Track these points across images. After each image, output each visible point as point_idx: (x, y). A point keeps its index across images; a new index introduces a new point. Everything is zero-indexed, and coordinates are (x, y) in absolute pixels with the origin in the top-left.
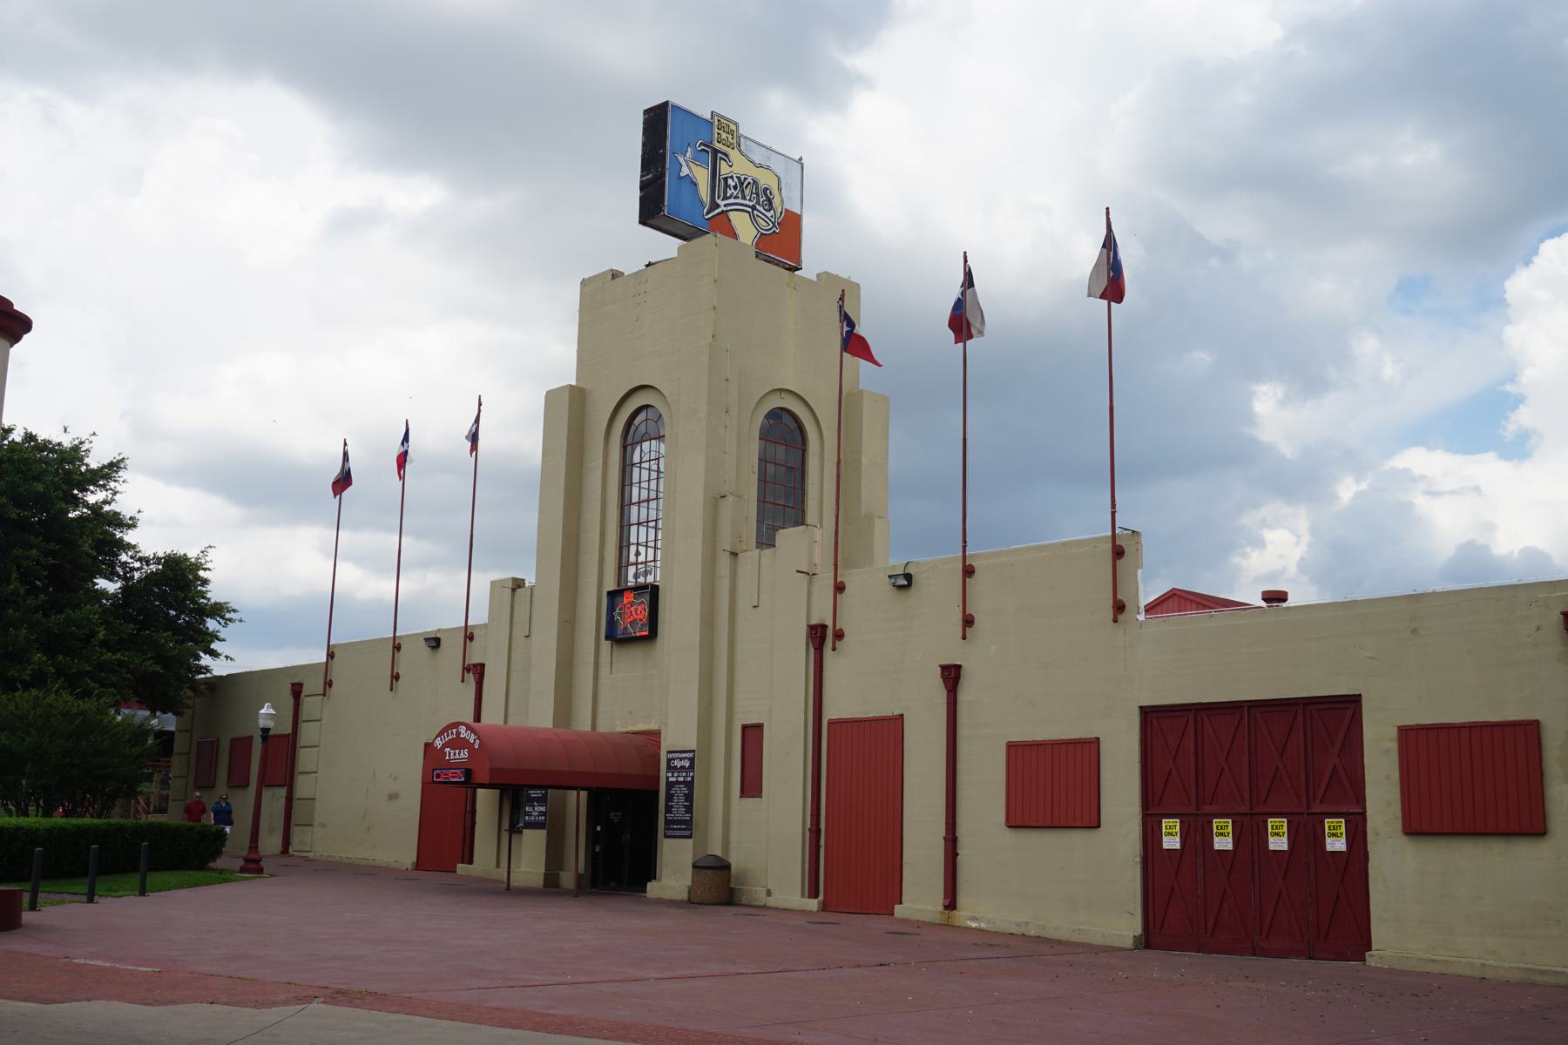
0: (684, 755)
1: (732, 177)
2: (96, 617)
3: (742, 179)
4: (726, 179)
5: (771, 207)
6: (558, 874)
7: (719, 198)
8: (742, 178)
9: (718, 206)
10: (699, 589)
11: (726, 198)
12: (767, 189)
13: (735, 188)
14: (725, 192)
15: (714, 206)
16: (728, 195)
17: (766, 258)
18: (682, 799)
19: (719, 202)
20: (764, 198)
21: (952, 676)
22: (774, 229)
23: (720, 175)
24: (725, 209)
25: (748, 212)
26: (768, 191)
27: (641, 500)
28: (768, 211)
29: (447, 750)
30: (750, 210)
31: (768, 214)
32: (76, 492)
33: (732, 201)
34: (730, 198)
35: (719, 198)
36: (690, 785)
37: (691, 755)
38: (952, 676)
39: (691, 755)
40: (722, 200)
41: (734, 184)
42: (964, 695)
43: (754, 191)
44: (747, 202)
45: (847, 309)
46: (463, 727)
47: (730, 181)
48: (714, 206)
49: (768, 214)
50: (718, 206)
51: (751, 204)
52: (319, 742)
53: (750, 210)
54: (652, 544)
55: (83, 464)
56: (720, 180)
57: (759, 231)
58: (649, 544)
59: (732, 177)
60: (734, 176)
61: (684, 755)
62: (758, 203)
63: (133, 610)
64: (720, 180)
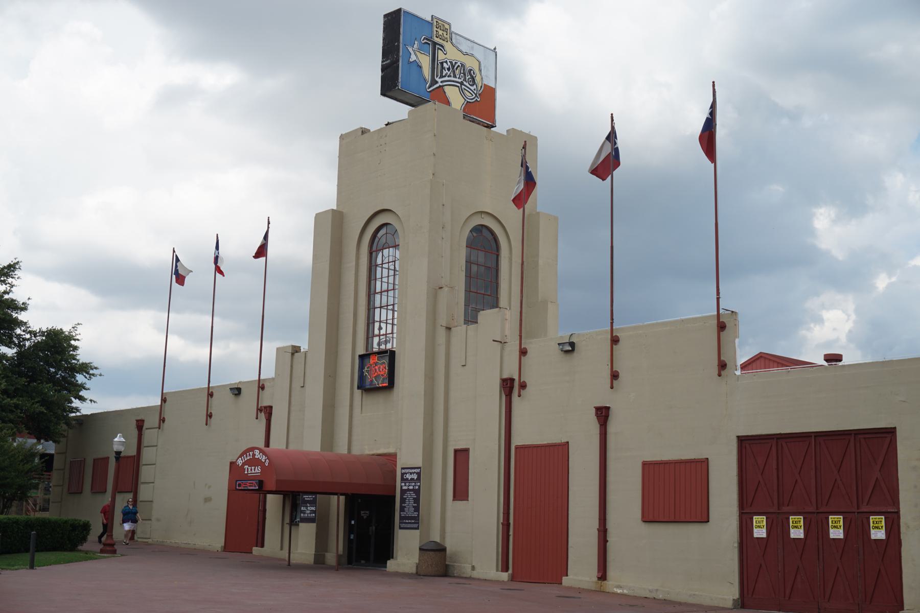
0: (413, 471)
4: (442, 63)
9: (437, 82)
14: (442, 72)
18: (412, 502)
19: (437, 79)
20: (469, 77)
21: (603, 414)
26: (472, 72)
29: (246, 467)
34: (445, 76)
36: (417, 492)
37: (418, 470)
38: (603, 414)
39: (418, 470)
42: (612, 428)
43: (462, 72)
46: (257, 451)
47: (445, 65)
61: (413, 471)
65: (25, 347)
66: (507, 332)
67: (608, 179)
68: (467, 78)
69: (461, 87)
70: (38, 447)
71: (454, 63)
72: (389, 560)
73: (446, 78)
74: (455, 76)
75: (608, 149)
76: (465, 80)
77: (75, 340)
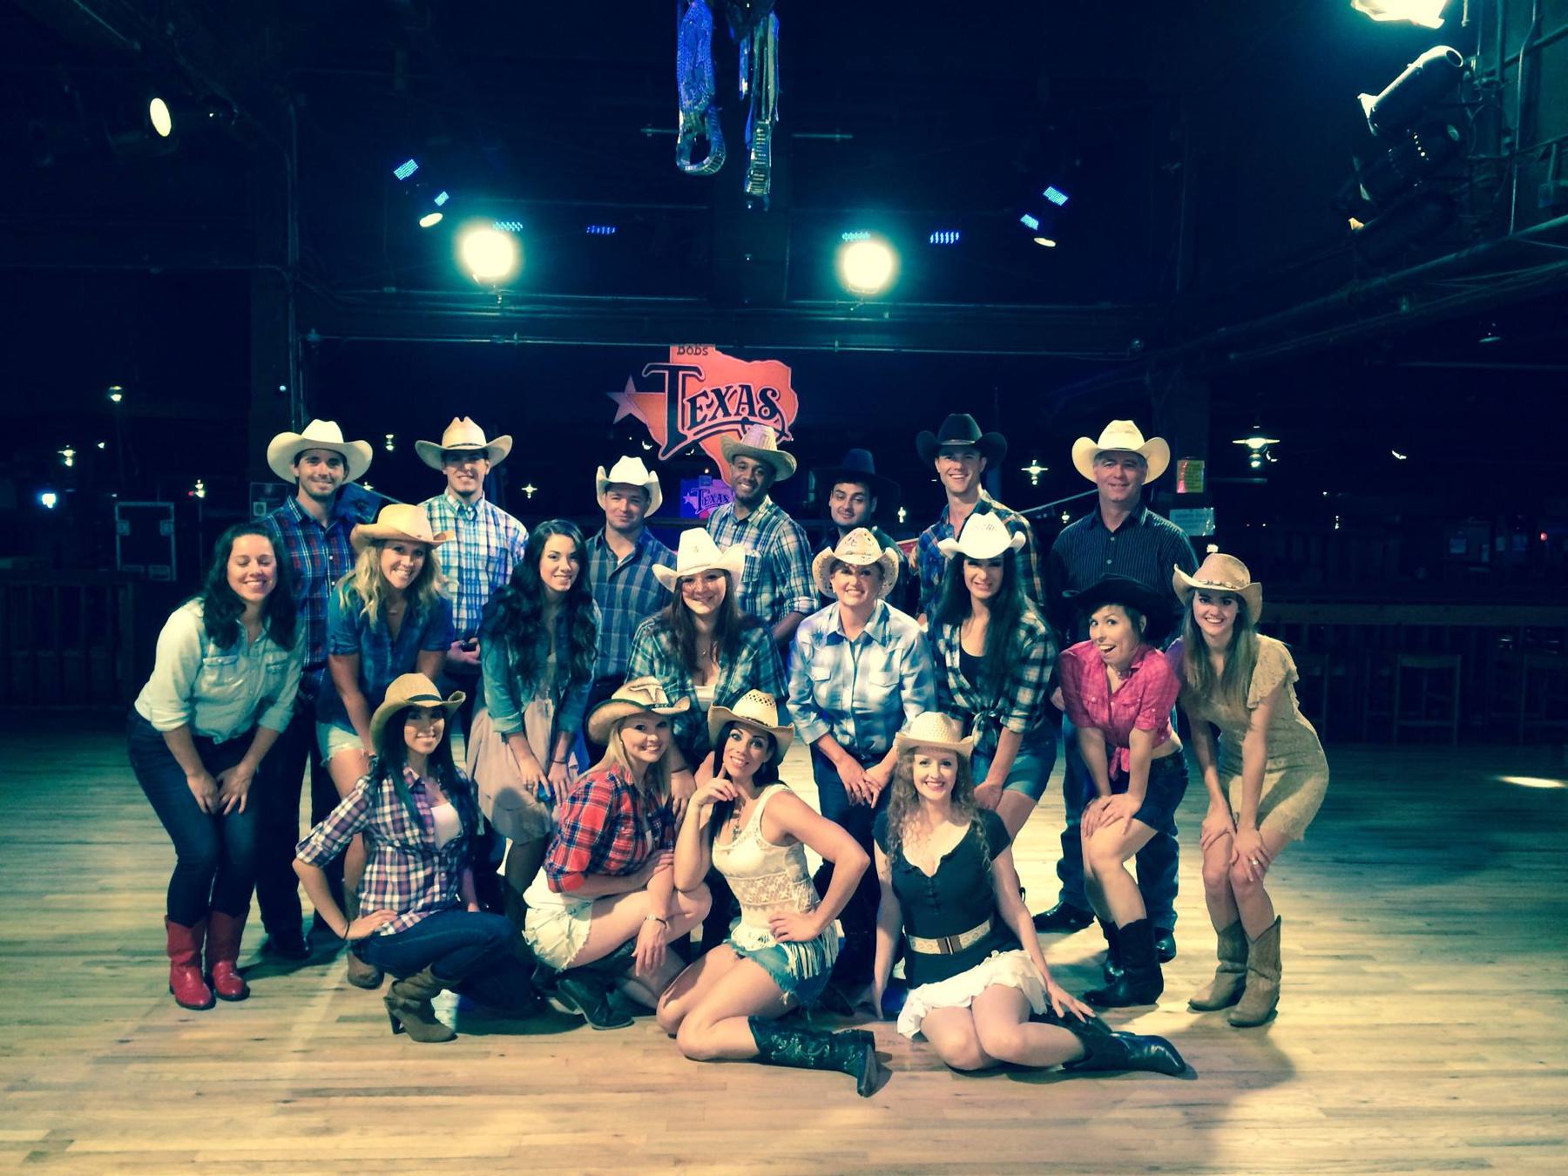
1: (705, 394)
2: (362, 817)
4: (693, 401)
6: (586, 1022)
9: (685, 438)
10: (1056, 1084)
14: (694, 416)
17: (118, 1159)
19: (685, 432)
20: (762, 404)
26: (769, 393)
32: (766, 209)
34: (703, 421)
40: (689, 429)
43: (745, 399)
47: (701, 401)
52: (253, 997)
53: (739, 427)
58: (578, 835)
59: (705, 394)
65: (317, 523)
66: (316, 972)
67: (814, 788)
68: (757, 408)
69: (743, 428)
70: (464, 626)
71: (724, 391)
72: (1062, 892)
73: (707, 424)
74: (729, 415)
75: (246, 727)
76: (752, 413)
77: (1515, 1042)
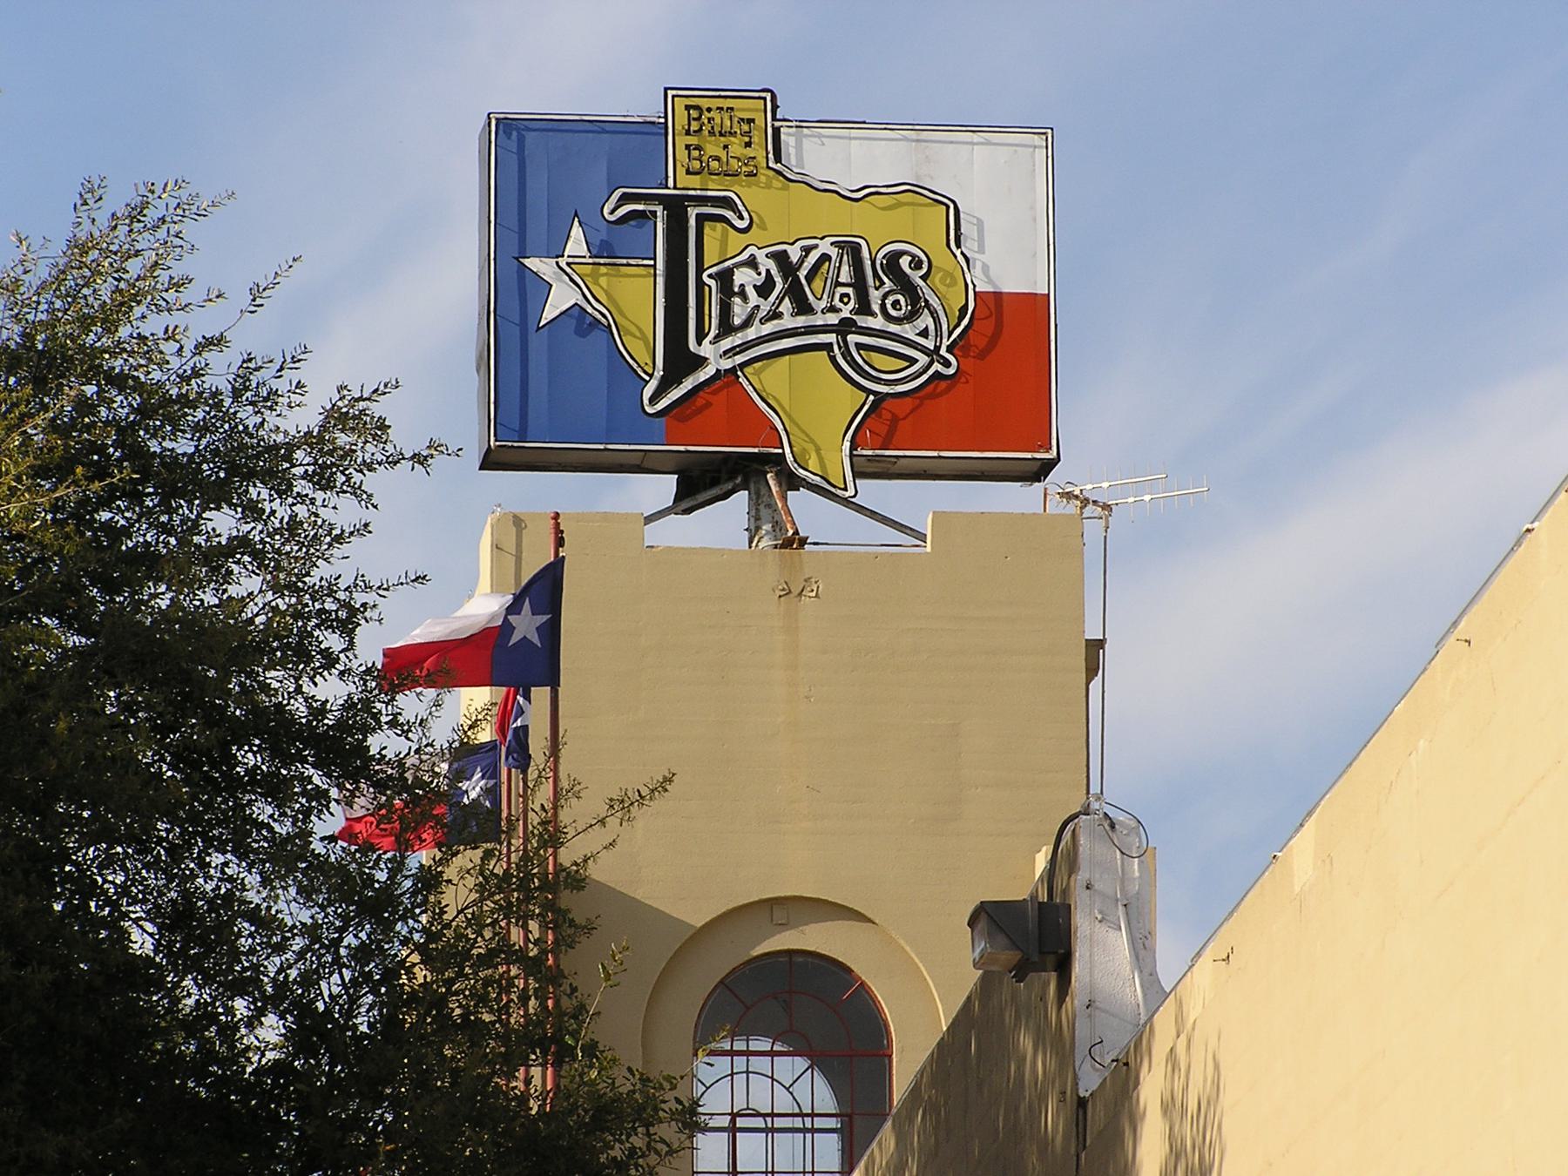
3: (794, 258)
5: (917, 305)
7: (700, 338)
8: (794, 254)
9: (701, 362)
11: (726, 328)
12: (894, 257)
13: (764, 290)
15: (680, 361)
16: (737, 321)
22: (937, 367)
23: (700, 269)
24: (727, 364)
25: (828, 347)
26: (904, 262)
27: (730, 1078)
28: (911, 317)
30: (831, 338)
31: (908, 331)
33: (751, 333)
34: (747, 324)
35: (700, 338)
41: (760, 280)
44: (819, 320)
45: (881, 206)
47: (743, 277)
48: (680, 361)
49: (908, 331)
50: (701, 362)
51: (833, 319)
54: (808, 1121)
55: (259, 1083)
56: (700, 284)
57: (869, 392)
60: (761, 256)
62: (864, 308)
63: (484, 1152)
64: (700, 284)
